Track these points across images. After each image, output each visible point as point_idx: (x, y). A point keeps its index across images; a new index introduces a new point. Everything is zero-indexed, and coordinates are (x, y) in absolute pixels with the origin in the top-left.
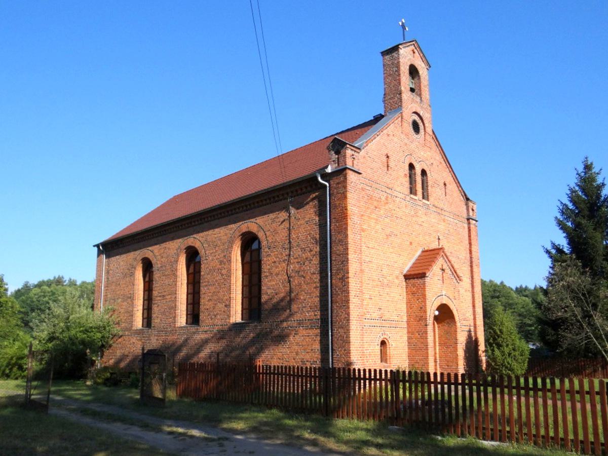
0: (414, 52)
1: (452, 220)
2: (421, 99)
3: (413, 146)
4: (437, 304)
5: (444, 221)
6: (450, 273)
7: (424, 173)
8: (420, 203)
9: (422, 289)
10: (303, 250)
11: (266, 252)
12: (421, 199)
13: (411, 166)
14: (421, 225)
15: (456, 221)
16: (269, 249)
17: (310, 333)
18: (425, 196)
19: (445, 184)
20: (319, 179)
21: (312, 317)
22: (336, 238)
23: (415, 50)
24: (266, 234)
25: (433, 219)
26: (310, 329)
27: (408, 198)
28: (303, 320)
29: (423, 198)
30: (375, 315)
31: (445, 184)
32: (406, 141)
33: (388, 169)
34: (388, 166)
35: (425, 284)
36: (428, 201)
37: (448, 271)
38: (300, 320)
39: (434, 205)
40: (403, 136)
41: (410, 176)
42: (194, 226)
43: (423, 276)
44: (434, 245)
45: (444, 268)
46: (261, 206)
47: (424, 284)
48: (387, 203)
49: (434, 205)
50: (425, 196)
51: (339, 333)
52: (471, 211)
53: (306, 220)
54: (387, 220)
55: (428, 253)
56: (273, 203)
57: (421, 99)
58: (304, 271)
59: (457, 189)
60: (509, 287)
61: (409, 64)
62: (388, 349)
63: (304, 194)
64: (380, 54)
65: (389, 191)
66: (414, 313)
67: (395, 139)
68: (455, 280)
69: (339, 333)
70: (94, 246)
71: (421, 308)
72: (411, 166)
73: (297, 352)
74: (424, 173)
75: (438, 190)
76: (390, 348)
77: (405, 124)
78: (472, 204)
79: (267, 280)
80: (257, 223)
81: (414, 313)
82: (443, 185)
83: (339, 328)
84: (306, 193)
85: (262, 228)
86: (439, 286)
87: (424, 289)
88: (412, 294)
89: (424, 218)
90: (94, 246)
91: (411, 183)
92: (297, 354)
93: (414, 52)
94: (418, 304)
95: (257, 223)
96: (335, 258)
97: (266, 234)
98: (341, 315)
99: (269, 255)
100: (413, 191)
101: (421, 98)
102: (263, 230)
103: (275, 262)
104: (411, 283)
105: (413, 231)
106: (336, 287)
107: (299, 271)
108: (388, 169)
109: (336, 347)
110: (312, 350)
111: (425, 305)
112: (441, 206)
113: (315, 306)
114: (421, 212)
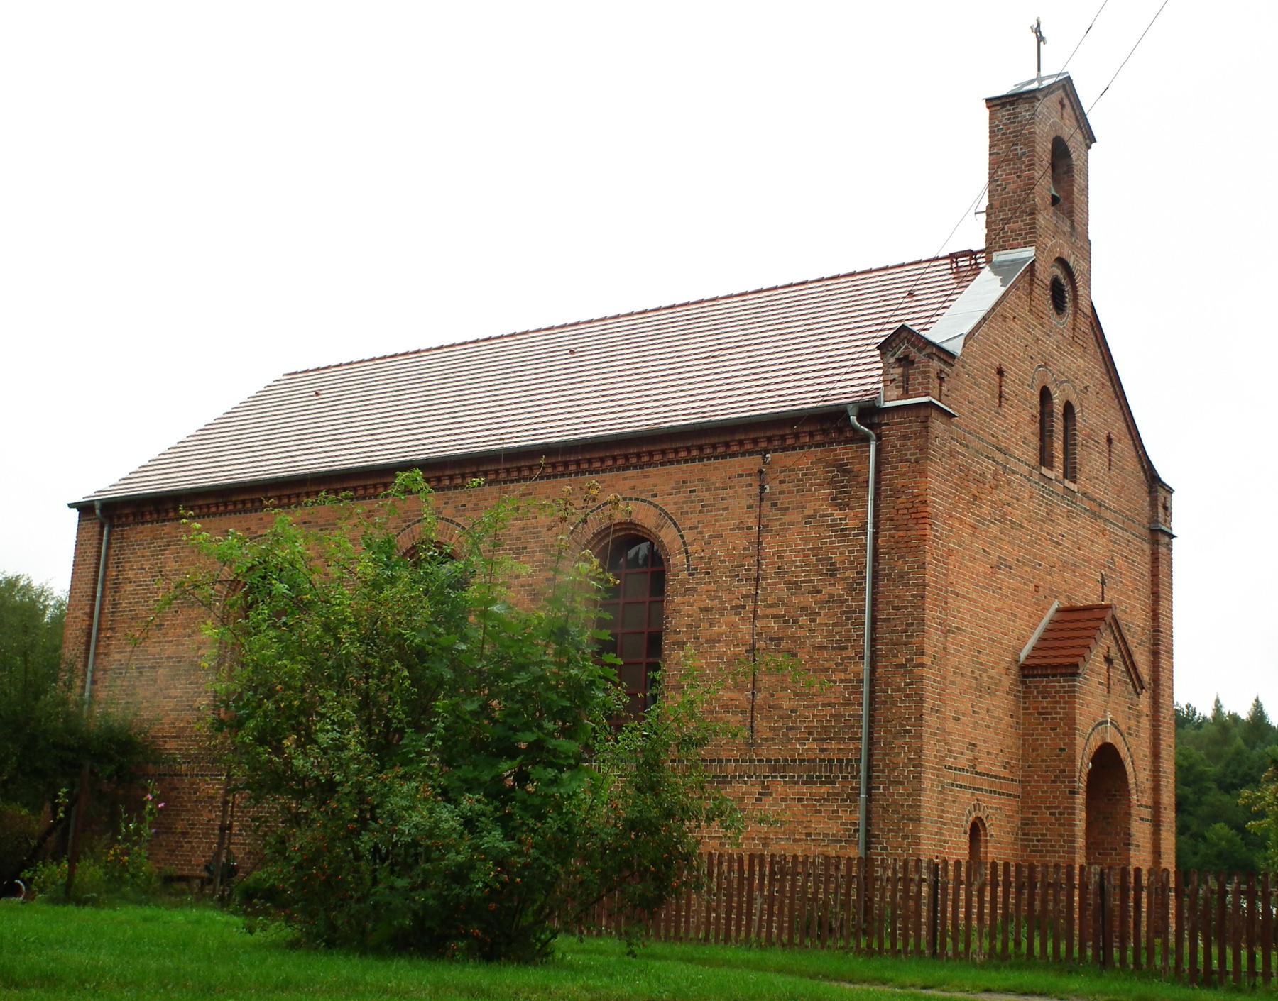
0: (1063, 106)
1: (1120, 532)
2: (1072, 227)
3: (1050, 343)
4: (1095, 743)
5: (1103, 532)
6: (1122, 668)
7: (1068, 409)
8: (1058, 488)
9: (1065, 703)
10: (793, 586)
11: (682, 583)
12: (1061, 476)
13: (1045, 395)
14: (1057, 543)
15: (1127, 535)
16: (691, 574)
17: (803, 794)
18: (1070, 472)
19: (1109, 440)
20: (853, 419)
21: (811, 755)
22: (892, 569)
23: (1066, 102)
24: (682, 537)
25: (1083, 526)
26: (804, 783)
27: (1036, 478)
28: (786, 760)
29: (1065, 476)
30: (963, 761)
31: (1109, 440)
32: (1038, 333)
33: (1000, 405)
34: (1000, 396)
35: (1074, 691)
36: (1075, 482)
37: (1118, 663)
38: (777, 761)
39: (1084, 494)
40: (1032, 320)
41: (1042, 422)
42: (449, 488)
43: (1071, 671)
44: (1088, 595)
45: (1112, 654)
46: (671, 463)
47: (1072, 691)
48: (996, 487)
49: (1084, 494)
50: (1070, 472)
51: (892, 795)
52: (1161, 510)
53: (807, 512)
54: (994, 529)
55: (1075, 616)
56: (709, 459)
57: (1072, 227)
58: (794, 638)
59: (1134, 454)
60: (112, 520)
61: (1053, 135)
62: (982, 844)
63: (802, 448)
64: (984, 104)
65: (1000, 458)
66: (1043, 761)
67: (1016, 327)
68: (1131, 688)
69: (892, 795)
70: (71, 506)
71: (1062, 750)
72: (1045, 395)
73: (766, 838)
74: (1068, 409)
75: (1095, 455)
76: (986, 841)
77: (1038, 291)
78: (1164, 493)
79: (682, 653)
80: (656, 506)
81: (1043, 761)
82: (1103, 441)
83: (891, 783)
84: (810, 447)
85: (671, 519)
86: (1101, 700)
87: (1071, 702)
88: (1040, 714)
89: (1064, 525)
90: (71, 506)
91: (1042, 439)
92: (765, 845)
93: (1063, 106)
94: (1052, 739)
95: (656, 506)
96: (888, 614)
97: (682, 537)
98: (899, 754)
99: (692, 590)
100: (1045, 459)
101: (1072, 221)
102: (676, 525)
103: (706, 609)
104: (1037, 687)
105: (1043, 558)
106: (887, 685)
107: (782, 639)
108: (1000, 405)
109: (881, 830)
110: (809, 835)
111: (1072, 744)
112: (1099, 495)
113: (822, 727)
114: (1061, 508)
